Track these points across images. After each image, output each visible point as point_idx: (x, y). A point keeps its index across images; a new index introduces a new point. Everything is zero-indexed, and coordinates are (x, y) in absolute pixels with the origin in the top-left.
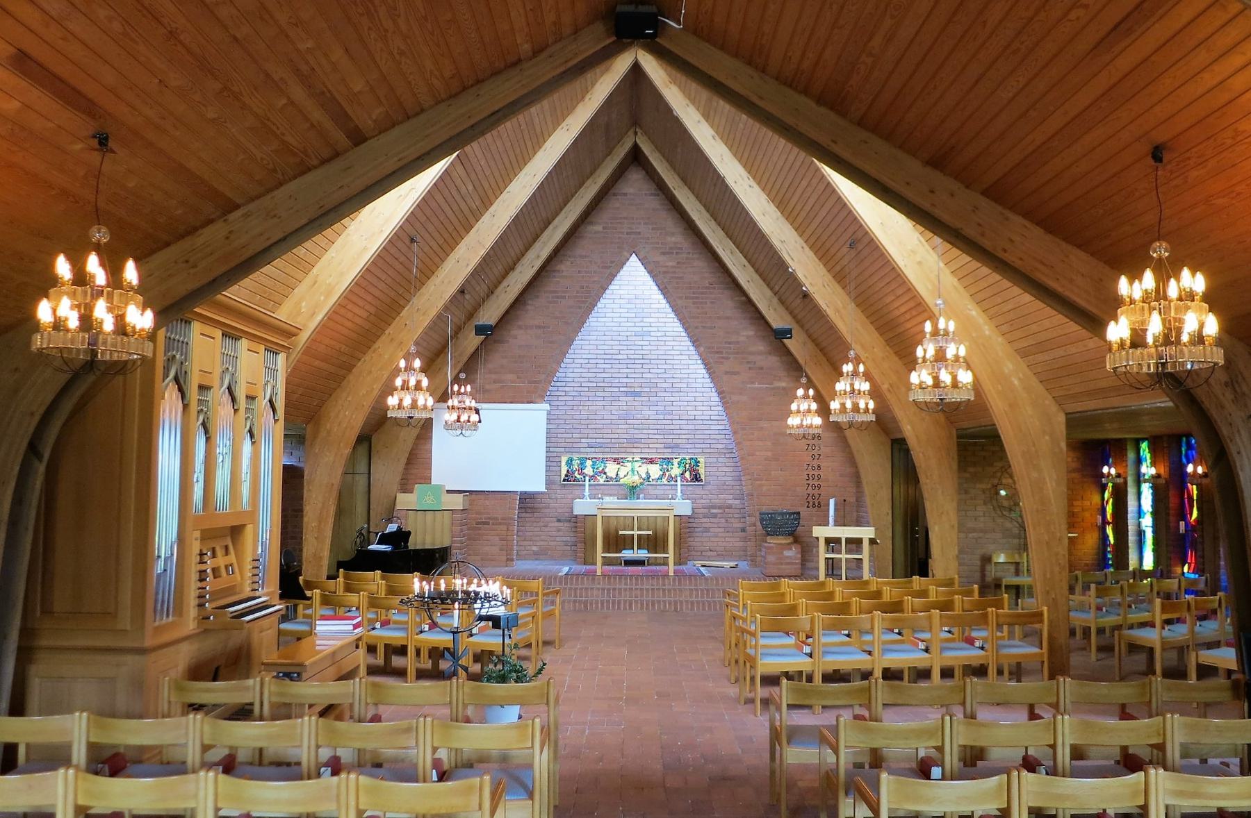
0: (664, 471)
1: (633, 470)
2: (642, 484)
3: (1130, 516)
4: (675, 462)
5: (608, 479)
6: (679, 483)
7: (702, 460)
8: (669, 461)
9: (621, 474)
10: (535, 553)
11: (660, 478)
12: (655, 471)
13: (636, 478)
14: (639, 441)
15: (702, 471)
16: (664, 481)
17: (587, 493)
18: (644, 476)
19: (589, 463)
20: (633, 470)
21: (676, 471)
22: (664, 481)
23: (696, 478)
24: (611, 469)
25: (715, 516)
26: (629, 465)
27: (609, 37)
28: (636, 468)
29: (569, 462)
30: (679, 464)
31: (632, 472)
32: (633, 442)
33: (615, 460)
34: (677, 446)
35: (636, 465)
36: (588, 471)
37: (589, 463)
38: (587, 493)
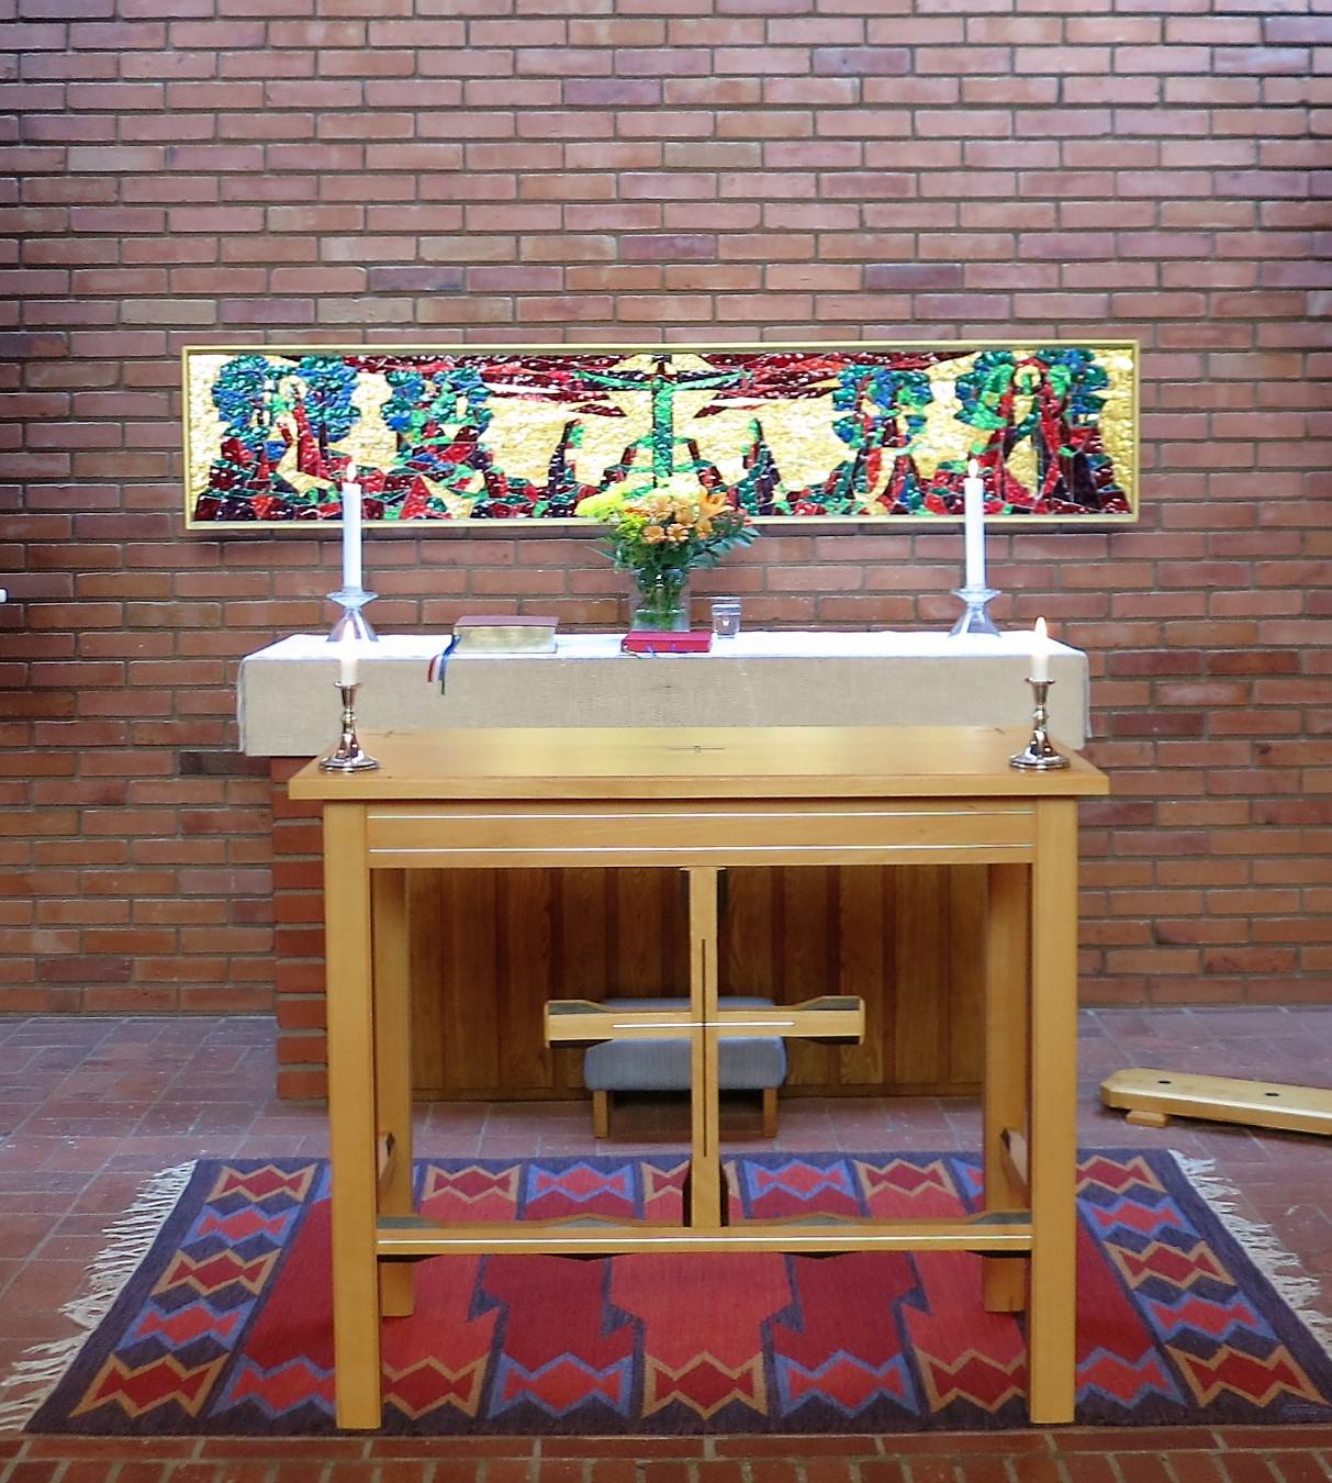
0: (873, 438)
1: (661, 436)
2: (725, 528)
3: (693, 955)
4: (943, 379)
5: (502, 495)
6: (975, 518)
7: (1118, 363)
8: (904, 371)
9: (588, 465)
10: (51, 970)
11: (844, 483)
12: (806, 438)
13: (685, 488)
14: (695, 247)
15: (1119, 430)
16: (871, 507)
17: (353, 596)
18: (733, 472)
19: (372, 391)
20: (661, 436)
21: (944, 436)
22: (871, 507)
23: (1081, 480)
24: (521, 432)
25: (1189, 724)
26: (636, 402)
27: (479, 1132)
28: (686, 427)
29: (235, 398)
30: (967, 392)
31: (649, 449)
32: (664, 257)
33: (542, 371)
34: (946, 277)
35: (686, 402)
36: (370, 445)
37: (372, 391)
38: (353, 596)
